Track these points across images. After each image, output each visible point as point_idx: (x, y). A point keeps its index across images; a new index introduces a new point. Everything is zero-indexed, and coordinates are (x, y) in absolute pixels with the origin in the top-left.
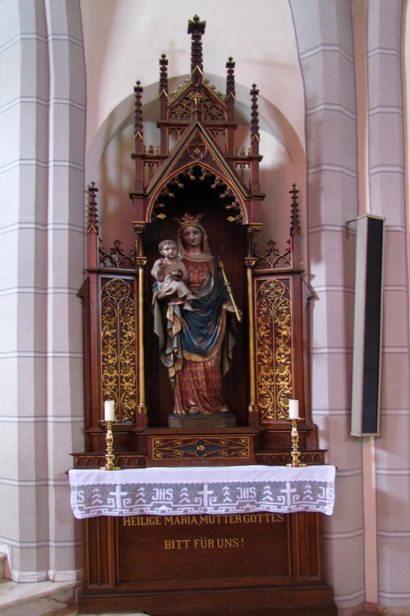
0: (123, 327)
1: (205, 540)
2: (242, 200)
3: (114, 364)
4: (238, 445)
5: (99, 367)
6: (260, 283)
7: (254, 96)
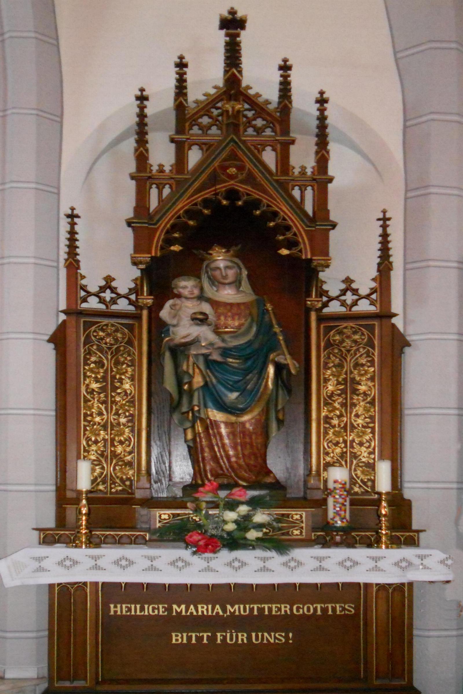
0: (116, 381)
1: (234, 634)
2: (301, 230)
3: (101, 424)
4: (288, 522)
5: (79, 427)
6: (328, 329)
7: (142, 103)
